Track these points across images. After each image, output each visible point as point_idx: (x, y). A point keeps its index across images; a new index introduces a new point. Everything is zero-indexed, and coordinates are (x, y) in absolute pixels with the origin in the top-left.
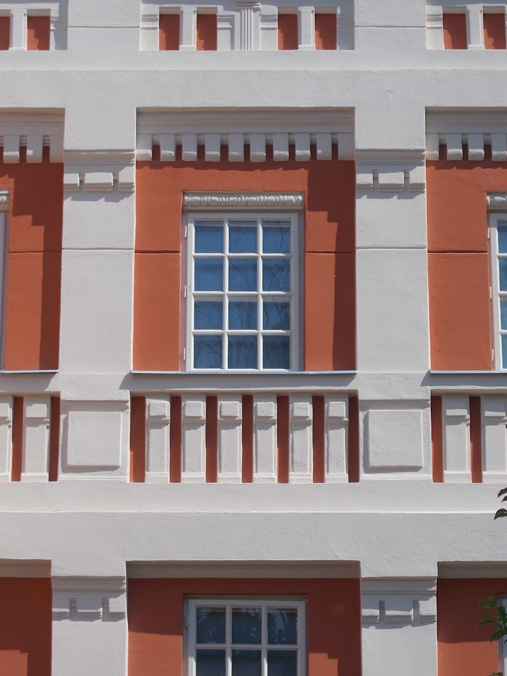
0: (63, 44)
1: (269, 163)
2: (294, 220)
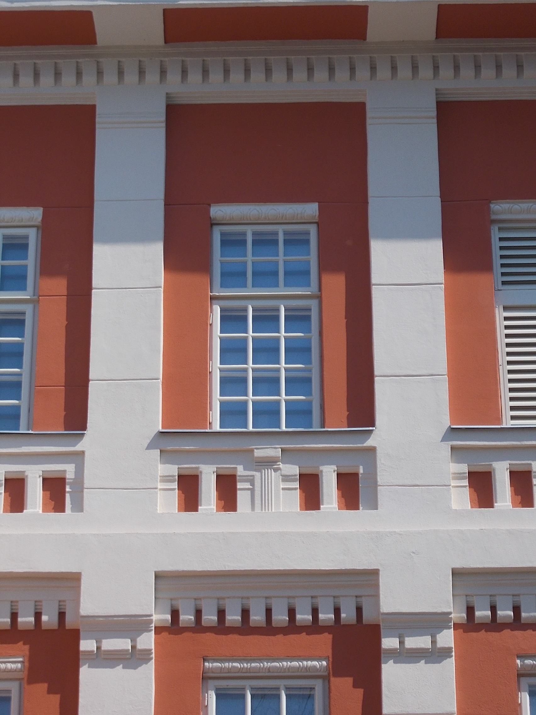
0: (79, 507)
1: (292, 627)
2: (318, 685)
